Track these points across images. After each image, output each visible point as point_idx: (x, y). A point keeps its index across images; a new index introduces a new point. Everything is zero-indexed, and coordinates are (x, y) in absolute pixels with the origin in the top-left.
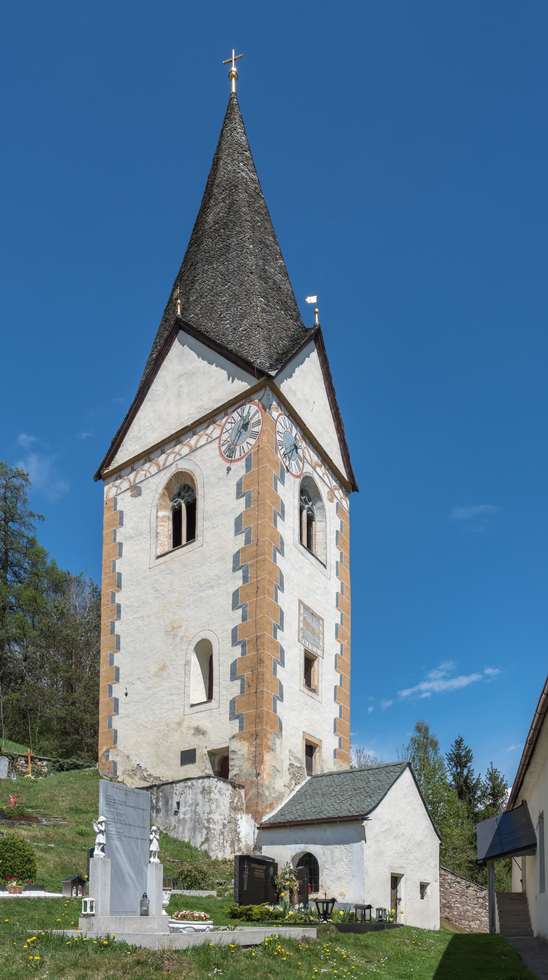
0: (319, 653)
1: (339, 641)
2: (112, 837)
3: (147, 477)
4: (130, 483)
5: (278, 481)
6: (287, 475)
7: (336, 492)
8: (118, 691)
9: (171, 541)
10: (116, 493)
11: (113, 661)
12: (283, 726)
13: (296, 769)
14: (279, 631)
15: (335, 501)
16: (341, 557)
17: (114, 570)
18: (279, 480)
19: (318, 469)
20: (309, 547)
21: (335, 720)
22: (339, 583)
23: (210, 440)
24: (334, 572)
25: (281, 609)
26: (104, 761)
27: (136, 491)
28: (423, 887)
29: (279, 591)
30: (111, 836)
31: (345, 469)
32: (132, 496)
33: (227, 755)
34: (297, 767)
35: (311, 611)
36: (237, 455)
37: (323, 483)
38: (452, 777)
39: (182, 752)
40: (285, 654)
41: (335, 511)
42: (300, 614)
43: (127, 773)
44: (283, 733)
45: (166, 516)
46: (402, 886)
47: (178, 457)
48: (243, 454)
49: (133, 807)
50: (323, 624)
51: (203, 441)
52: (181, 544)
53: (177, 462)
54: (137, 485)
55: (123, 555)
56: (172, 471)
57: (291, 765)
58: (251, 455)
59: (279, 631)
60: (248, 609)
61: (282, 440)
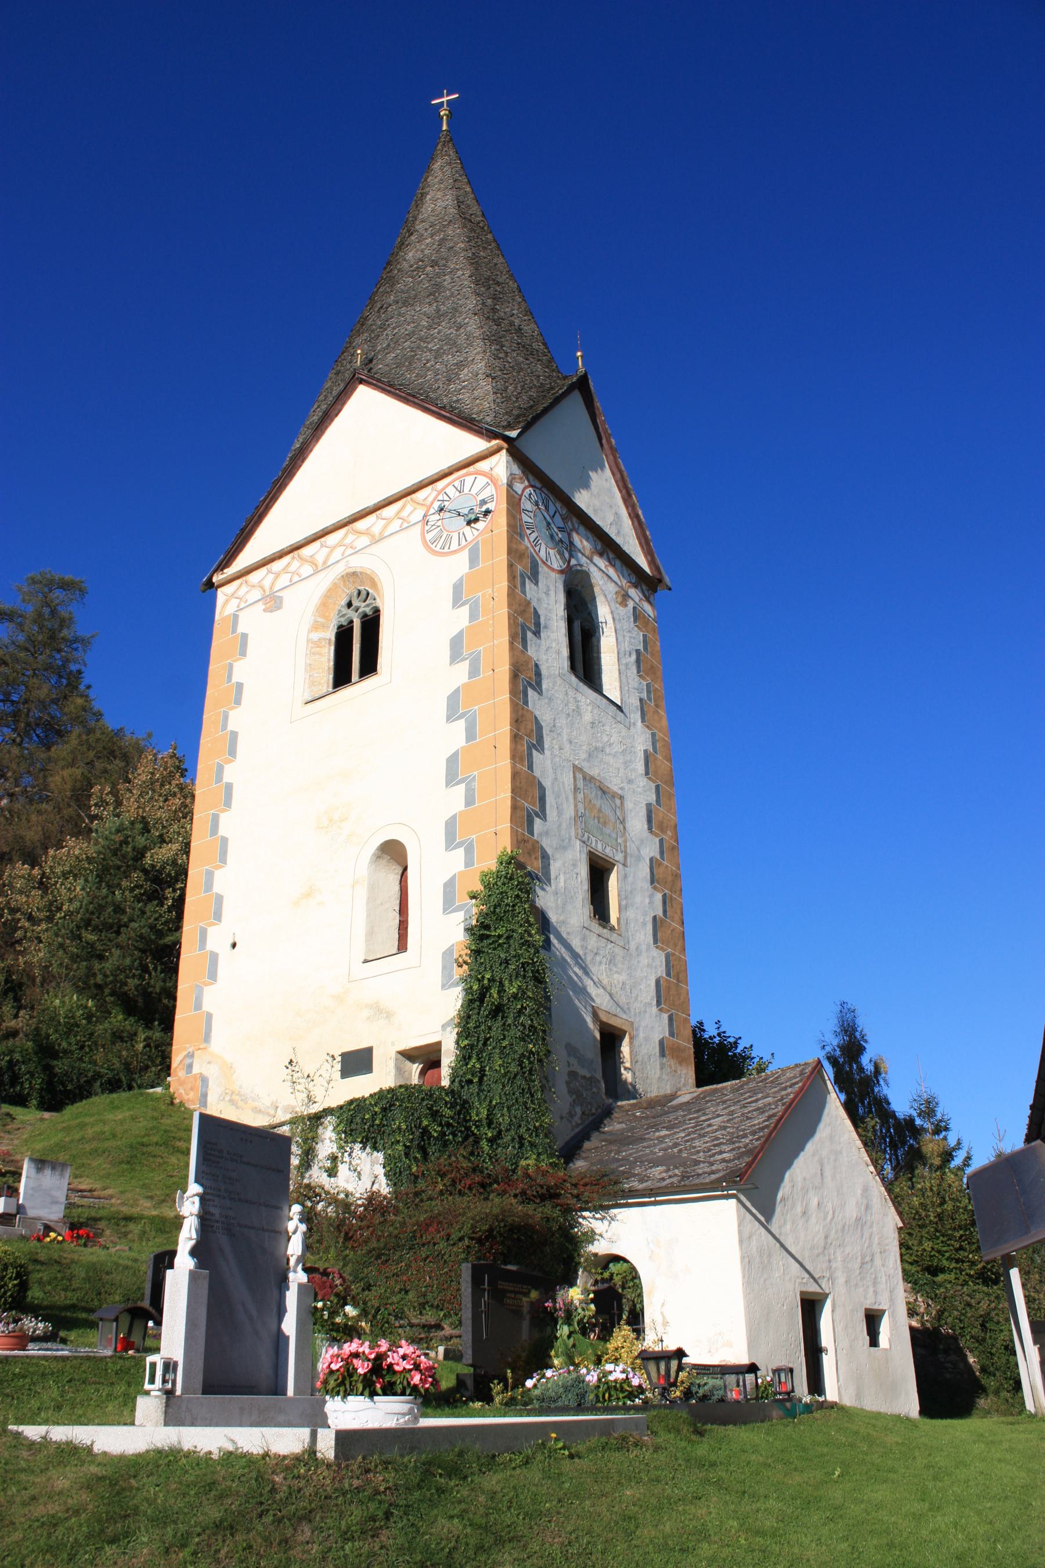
0: (619, 857)
2: (212, 1226)
4: (264, 591)
5: (527, 580)
6: (542, 569)
8: (217, 939)
9: (331, 677)
10: (238, 606)
11: (212, 884)
13: (582, 1081)
14: (538, 822)
17: (225, 726)
18: (529, 578)
21: (658, 982)
22: (648, 734)
23: (405, 525)
24: (638, 716)
25: (539, 782)
27: (273, 602)
28: (873, 1320)
29: (534, 752)
30: (212, 1224)
31: (646, 557)
32: (264, 610)
33: (436, 1059)
34: (584, 1077)
35: (598, 784)
36: (454, 546)
38: (142, 826)
42: (576, 789)
43: (228, 1098)
45: (325, 639)
47: (350, 551)
49: (256, 1166)
51: (396, 525)
52: (351, 681)
53: (348, 558)
55: (243, 702)
56: (340, 569)
57: (573, 1074)
58: (478, 543)
60: (476, 785)
61: (532, 521)
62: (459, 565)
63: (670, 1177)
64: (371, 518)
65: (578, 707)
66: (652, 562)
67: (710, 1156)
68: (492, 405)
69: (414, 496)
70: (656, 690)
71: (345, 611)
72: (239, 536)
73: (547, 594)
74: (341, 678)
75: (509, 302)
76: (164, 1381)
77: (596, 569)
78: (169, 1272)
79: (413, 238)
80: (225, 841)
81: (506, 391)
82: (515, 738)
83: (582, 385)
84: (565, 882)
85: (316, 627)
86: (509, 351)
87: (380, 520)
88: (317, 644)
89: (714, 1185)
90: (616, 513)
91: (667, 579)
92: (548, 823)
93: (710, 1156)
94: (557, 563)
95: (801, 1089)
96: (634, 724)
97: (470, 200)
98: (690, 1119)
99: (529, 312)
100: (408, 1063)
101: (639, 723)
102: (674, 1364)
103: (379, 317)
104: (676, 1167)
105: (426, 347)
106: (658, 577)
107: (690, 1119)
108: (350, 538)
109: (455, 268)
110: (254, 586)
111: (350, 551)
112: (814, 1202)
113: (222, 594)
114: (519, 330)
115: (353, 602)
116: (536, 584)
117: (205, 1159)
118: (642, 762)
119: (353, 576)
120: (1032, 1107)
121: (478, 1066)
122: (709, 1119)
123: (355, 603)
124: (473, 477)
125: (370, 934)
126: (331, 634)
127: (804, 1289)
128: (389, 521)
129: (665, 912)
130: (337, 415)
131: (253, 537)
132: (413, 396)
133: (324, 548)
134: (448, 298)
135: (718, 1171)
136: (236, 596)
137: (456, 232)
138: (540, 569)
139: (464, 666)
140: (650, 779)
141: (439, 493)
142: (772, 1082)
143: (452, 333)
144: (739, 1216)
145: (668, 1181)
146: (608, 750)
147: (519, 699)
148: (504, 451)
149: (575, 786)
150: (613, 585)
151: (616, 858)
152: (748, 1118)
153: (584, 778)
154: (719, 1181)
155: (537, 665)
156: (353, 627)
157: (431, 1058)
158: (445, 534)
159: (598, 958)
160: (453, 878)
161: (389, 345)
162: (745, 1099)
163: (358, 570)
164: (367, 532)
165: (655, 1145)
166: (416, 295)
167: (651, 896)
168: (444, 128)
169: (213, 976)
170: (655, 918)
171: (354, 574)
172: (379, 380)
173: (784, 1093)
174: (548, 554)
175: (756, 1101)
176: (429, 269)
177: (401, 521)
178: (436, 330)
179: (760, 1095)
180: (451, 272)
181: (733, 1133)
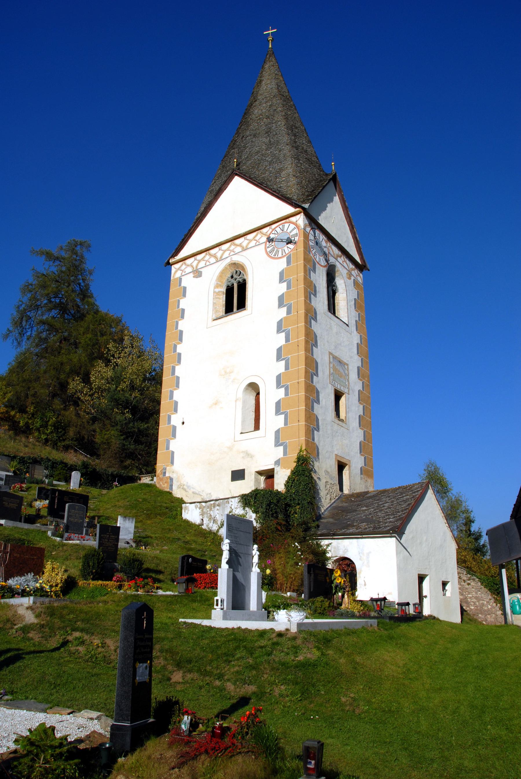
0: (346, 390)
1: (361, 380)
3: (207, 265)
5: (311, 271)
6: (317, 266)
7: (353, 272)
8: (175, 420)
12: (320, 451)
15: (353, 278)
16: (359, 317)
19: (339, 259)
20: (334, 313)
21: (360, 443)
23: (258, 243)
25: (316, 361)
26: (161, 476)
27: (198, 273)
29: (314, 347)
31: (359, 256)
32: (194, 277)
36: (280, 255)
37: (343, 267)
39: (232, 472)
40: (320, 394)
41: (353, 285)
42: (330, 362)
43: (182, 487)
44: (320, 457)
45: (221, 292)
46: (426, 584)
47: (232, 253)
48: (284, 254)
50: (348, 368)
51: (253, 243)
53: (232, 256)
54: (200, 270)
56: (228, 261)
59: (315, 377)
62: (282, 264)
63: (369, 528)
64: (242, 239)
65: (331, 326)
66: (362, 258)
67: (385, 520)
68: (296, 190)
69: (261, 230)
70: (362, 316)
71: (230, 279)
72: (181, 242)
73: (319, 277)
74: (229, 309)
75: (301, 137)
76: (221, 606)
77: (338, 263)
78: (219, 569)
79: (257, 103)
80: (178, 378)
81: (301, 183)
82: (307, 342)
83: (334, 179)
84: (325, 402)
85: (217, 286)
86: (302, 162)
87: (246, 240)
88: (218, 293)
89: (387, 532)
90: (347, 237)
91: (368, 266)
92: (319, 378)
93: (385, 520)
94: (323, 263)
95: (421, 493)
96: (353, 332)
97: (282, 85)
98: (375, 503)
99: (310, 142)
100: (260, 476)
101: (355, 331)
102: (383, 602)
103: (242, 141)
104: (371, 524)
105: (265, 159)
106: (364, 265)
107: (375, 503)
108: (233, 247)
109: (277, 121)
111: (232, 253)
112: (425, 538)
113: (174, 268)
114: (306, 151)
115: (234, 276)
116: (315, 273)
117: (228, 530)
118: (356, 349)
119: (234, 264)
120: (515, 505)
122: (383, 504)
123: (235, 276)
124: (288, 224)
125: (243, 422)
126: (224, 290)
127: (419, 573)
128: (250, 241)
129: (364, 413)
131: (188, 243)
132: (261, 184)
133: (221, 251)
134: (274, 135)
135: (389, 526)
137: (278, 102)
138: (316, 266)
139: (285, 309)
140: (359, 356)
141: (273, 230)
142: (409, 489)
143: (277, 153)
144: (396, 544)
145: (368, 530)
146: (342, 344)
147: (308, 325)
148: (302, 213)
149: (330, 360)
150: (345, 270)
151: (345, 391)
152: (400, 504)
153: (333, 357)
154: (389, 530)
155: (315, 309)
156: (234, 287)
157: (269, 474)
158: (276, 249)
159: (337, 434)
160: (280, 400)
161: (247, 157)
162: (398, 496)
163: (236, 262)
164: (240, 245)
165: (361, 514)
166: (259, 133)
167: (358, 407)
168: (270, 46)
169: (174, 435)
170: (360, 416)
171: (235, 264)
172: (245, 175)
173: (414, 494)
174: (320, 259)
175: (403, 497)
176: (265, 119)
177: (256, 241)
178: (270, 151)
179: (404, 495)
180: (275, 122)
181: (393, 510)
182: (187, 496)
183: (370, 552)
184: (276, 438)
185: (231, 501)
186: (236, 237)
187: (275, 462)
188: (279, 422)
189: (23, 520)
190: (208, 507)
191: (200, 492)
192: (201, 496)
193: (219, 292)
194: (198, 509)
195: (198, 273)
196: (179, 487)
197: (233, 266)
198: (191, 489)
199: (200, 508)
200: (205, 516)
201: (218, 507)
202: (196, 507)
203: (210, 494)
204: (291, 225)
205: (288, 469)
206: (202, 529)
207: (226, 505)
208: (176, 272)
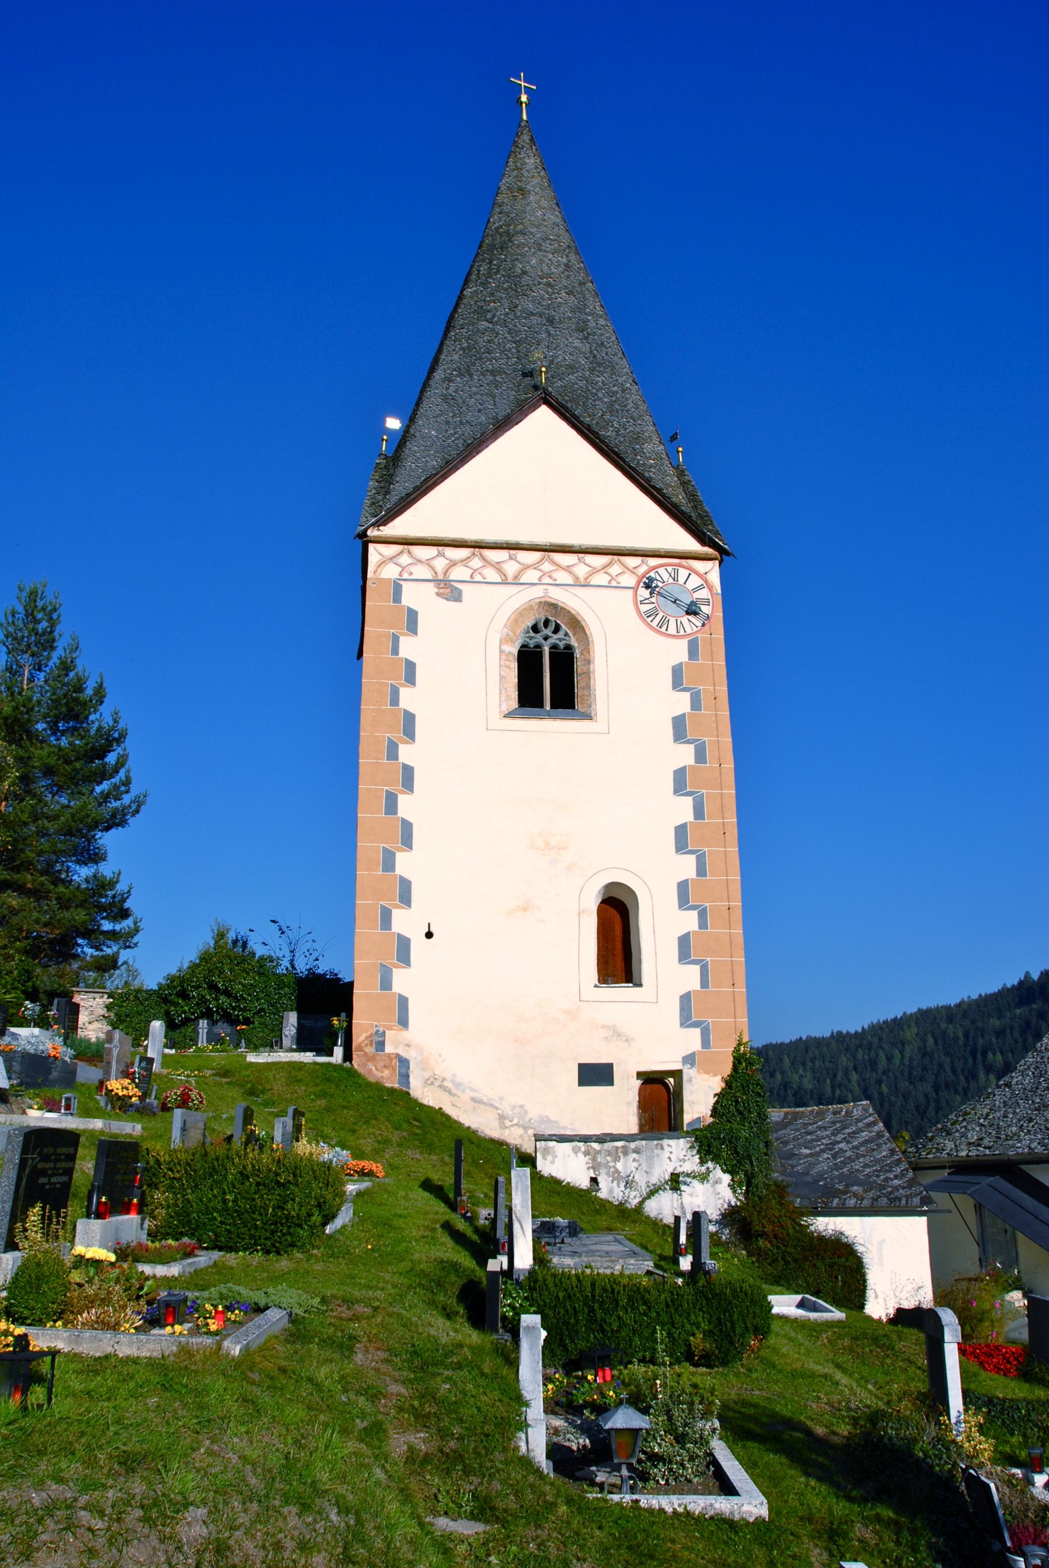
43: (437, 1083)
51: (601, 579)
54: (453, 583)
56: (537, 593)
87: (582, 565)
110: (421, 562)
121: (279, 1385)
130: (517, 424)
133: (513, 562)
136: (395, 560)
163: (560, 604)
182: (454, 1105)
183: (884, 1241)
184: (682, 1009)
185: (669, 1146)
186: (560, 549)
187: (683, 1058)
188: (690, 978)
189: (70, 1164)
190: (609, 1153)
191: (492, 1099)
192: (497, 1108)
193: (509, 653)
194: (581, 1155)
195: (450, 591)
196: (429, 1082)
197: (546, 608)
198: (467, 1091)
199: (586, 1153)
200: (603, 1171)
201: (635, 1155)
202: (576, 1151)
203: (521, 1107)
204: (693, 576)
205: (714, 1076)
206: (597, 1198)
207: (656, 1151)
208: (381, 564)
